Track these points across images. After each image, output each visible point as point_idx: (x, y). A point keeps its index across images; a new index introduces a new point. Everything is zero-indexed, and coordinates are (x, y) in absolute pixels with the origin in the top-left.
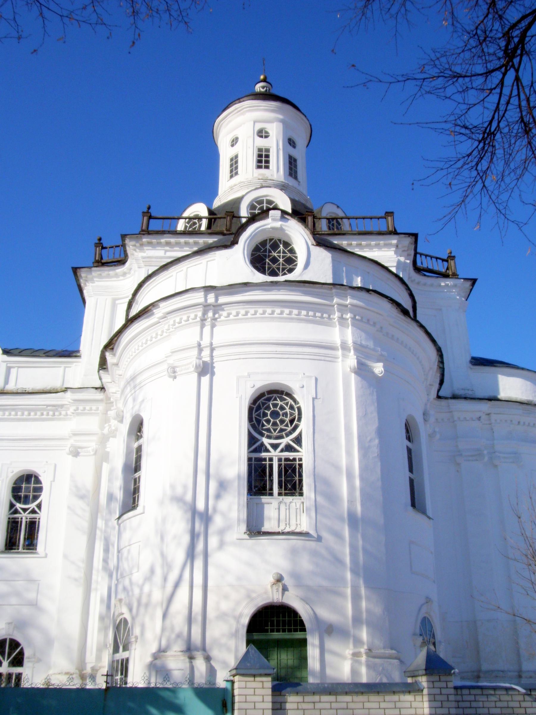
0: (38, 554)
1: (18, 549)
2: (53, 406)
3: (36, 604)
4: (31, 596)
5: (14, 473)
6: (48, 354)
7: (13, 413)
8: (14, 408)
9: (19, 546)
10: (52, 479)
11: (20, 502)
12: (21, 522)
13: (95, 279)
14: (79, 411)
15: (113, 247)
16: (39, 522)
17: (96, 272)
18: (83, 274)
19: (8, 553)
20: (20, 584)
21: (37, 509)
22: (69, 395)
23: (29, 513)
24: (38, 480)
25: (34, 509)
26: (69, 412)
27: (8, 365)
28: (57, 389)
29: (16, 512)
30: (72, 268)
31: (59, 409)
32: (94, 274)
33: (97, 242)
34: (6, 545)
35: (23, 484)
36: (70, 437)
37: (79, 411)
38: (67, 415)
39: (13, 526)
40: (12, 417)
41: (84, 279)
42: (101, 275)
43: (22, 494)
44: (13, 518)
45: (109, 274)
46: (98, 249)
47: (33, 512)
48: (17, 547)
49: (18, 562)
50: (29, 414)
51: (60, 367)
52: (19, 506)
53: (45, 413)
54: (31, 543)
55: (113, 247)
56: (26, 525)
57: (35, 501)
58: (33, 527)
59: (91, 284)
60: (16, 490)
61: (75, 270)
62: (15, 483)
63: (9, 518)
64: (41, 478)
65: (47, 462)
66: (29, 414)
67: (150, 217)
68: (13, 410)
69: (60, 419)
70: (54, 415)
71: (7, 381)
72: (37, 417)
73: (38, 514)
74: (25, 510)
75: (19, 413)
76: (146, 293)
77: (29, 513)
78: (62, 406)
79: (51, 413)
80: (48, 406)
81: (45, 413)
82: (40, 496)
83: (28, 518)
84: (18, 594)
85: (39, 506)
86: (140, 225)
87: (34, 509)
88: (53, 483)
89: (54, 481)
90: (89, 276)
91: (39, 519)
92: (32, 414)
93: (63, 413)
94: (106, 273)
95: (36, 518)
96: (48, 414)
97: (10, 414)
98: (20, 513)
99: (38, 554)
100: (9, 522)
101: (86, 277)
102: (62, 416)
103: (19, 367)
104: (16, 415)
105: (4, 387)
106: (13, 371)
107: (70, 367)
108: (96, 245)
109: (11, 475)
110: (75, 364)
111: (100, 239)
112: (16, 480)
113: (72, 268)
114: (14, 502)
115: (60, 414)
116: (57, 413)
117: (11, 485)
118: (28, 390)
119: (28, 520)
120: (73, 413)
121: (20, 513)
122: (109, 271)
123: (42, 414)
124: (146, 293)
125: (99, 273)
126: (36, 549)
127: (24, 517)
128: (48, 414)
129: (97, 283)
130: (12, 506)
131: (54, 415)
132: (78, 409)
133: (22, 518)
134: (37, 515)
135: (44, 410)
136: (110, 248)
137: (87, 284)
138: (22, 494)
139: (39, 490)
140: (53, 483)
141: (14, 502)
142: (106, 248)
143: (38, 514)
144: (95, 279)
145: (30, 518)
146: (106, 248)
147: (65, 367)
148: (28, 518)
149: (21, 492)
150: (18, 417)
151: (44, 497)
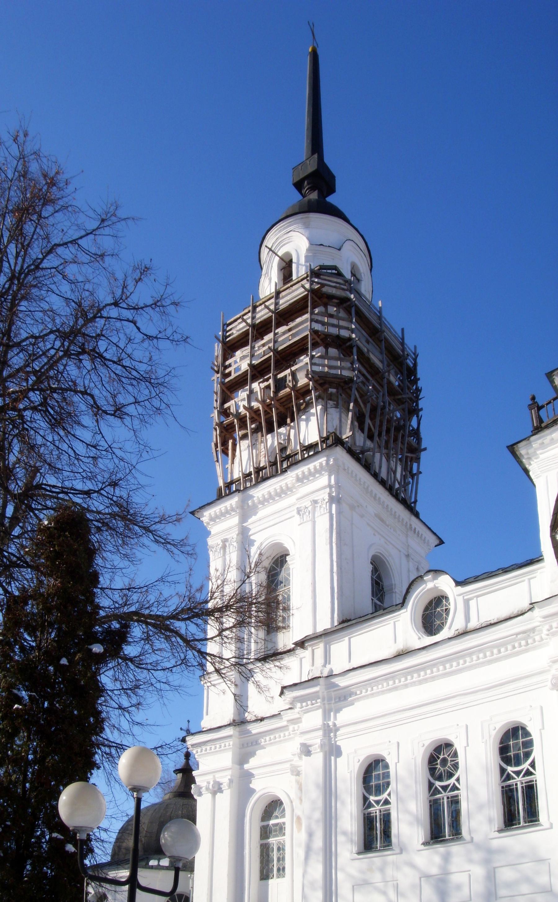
0: (542, 825)
1: (519, 823)
2: (524, 632)
3: (551, 891)
4: (543, 880)
5: (497, 729)
6: (506, 570)
7: (481, 655)
8: (481, 648)
9: (519, 820)
10: (541, 727)
11: (511, 766)
12: (517, 789)
13: (538, 452)
14: (554, 629)
15: (550, 402)
16: (536, 784)
17: (537, 441)
18: (522, 450)
19: (507, 830)
20: (528, 868)
21: (531, 769)
22: (537, 613)
23: (524, 776)
24: (526, 733)
25: (528, 769)
26: (544, 636)
27: (465, 598)
28: (522, 611)
29: (509, 777)
30: (508, 447)
31: (532, 635)
32: (535, 445)
33: (531, 402)
34: (505, 822)
35: (510, 741)
36: (550, 666)
37: (554, 629)
38: (542, 639)
39: (508, 795)
40: (481, 660)
41: (526, 457)
42: (543, 443)
43: (512, 754)
44: (506, 786)
45: (552, 439)
46: (533, 411)
47: (528, 773)
48: (517, 822)
49: (522, 839)
50: (499, 652)
51: (523, 581)
52: (510, 769)
53: (516, 645)
54: (532, 815)
55: (550, 402)
56: (523, 792)
57: (526, 761)
58: (530, 791)
59: (535, 460)
60: (504, 750)
61: (512, 449)
62: (501, 742)
63: (503, 787)
64: (529, 729)
65: (531, 706)
66: (499, 652)
67: (540, 408)
68: (480, 651)
69: (534, 648)
70: (527, 644)
71: (467, 619)
72: (509, 652)
73: (534, 774)
74: (518, 773)
75: (488, 653)
76: (353, 784)
77: (524, 776)
78: (533, 630)
79: (523, 643)
80: (517, 634)
81: (516, 645)
82: (532, 751)
83: (524, 782)
84: (528, 880)
85: (533, 765)
86: (531, 425)
87: (528, 769)
88: (542, 731)
89: (543, 729)
90: (531, 451)
91: (536, 781)
92: (503, 650)
93: (537, 638)
94: (549, 438)
95: (533, 781)
96: (520, 646)
97: (478, 658)
98: (514, 778)
99: (542, 825)
100: (502, 791)
101: (528, 454)
102: (537, 643)
103: (478, 597)
104: (485, 656)
105: (466, 627)
106: (472, 603)
107: (536, 577)
108: (530, 407)
109: (493, 733)
110: (539, 571)
111: (533, 398)
112: (502, 739)
113: (508, 447)
114: (504, 766)
115: (534, 641)
116: (530, 641)
117: (497, 746)
118: (492, 622)
119: (524, 785)
120: (548, 635)
121: (514, 778)
122: (551, 434)
123: (514, 647)
124: (353, 784)
125: (540, 441)
126: (539, 821)
127: (519, 782)
128: (520, 646)
129: (542, 456)
130: (503, 771)
131: (527, 644)
132: (551, 627)
133: (516, 785)
134: (533, 776)
135: (514, 640)
136: (547, 404)
137: (532, 462)
138: (512, 754)
139: (529, 744)
140: (542, 731)
141: (504, 766)
142: (543, 407)
143: (534, 774)
144: (538, 452)
145: (525, 783)
146: (543, 407)
147: (529, 579)
148: (524, 782)
149: (510, 752)
150: (488, 658)
151: (536, 754)
